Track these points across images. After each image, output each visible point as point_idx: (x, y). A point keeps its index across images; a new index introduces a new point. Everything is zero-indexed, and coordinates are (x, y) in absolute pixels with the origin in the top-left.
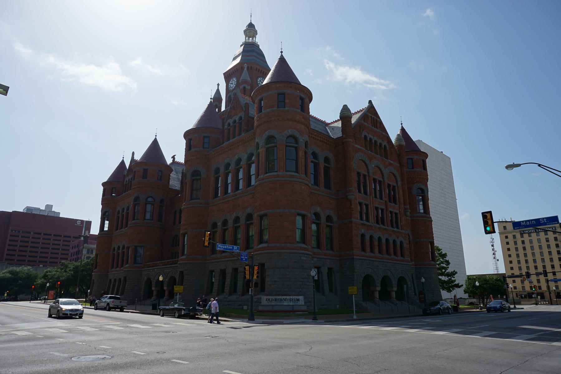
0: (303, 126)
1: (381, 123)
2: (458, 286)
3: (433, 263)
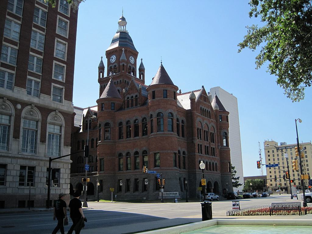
2: (240, 185)
3: (230, 173)
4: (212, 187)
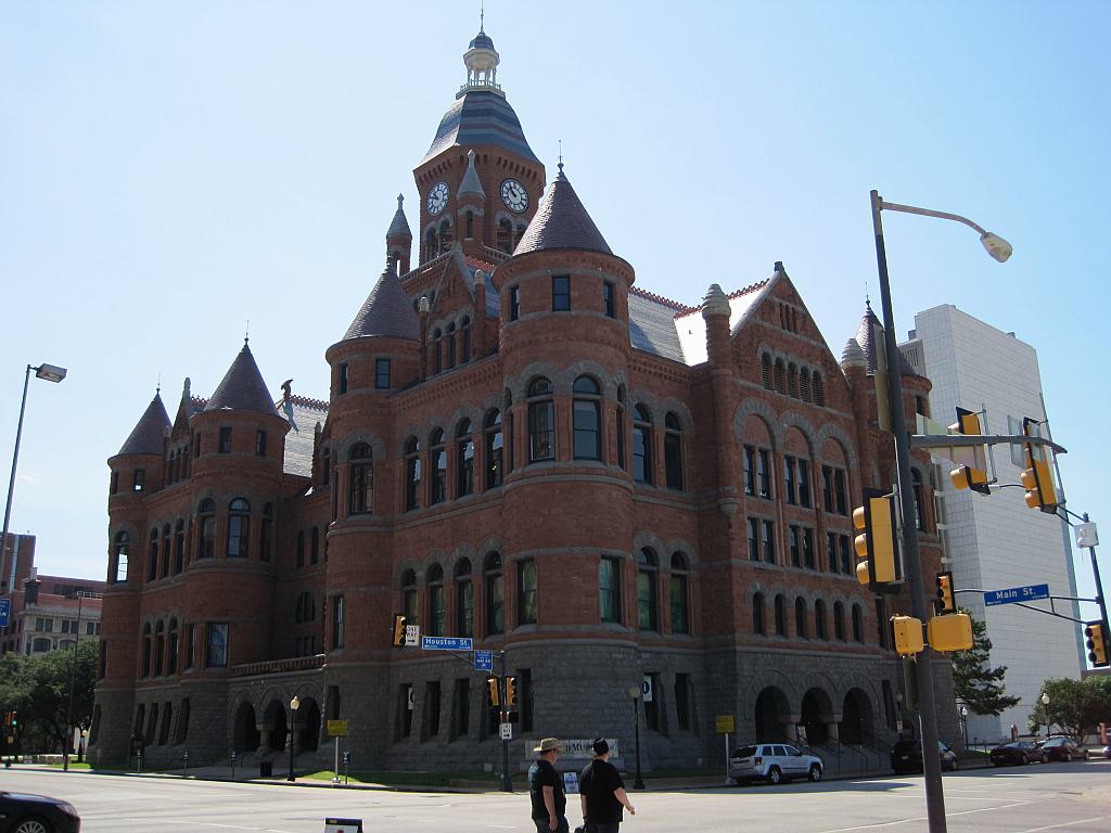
0: (610, 351)
1: (807, 316)
4: (831, 713)
